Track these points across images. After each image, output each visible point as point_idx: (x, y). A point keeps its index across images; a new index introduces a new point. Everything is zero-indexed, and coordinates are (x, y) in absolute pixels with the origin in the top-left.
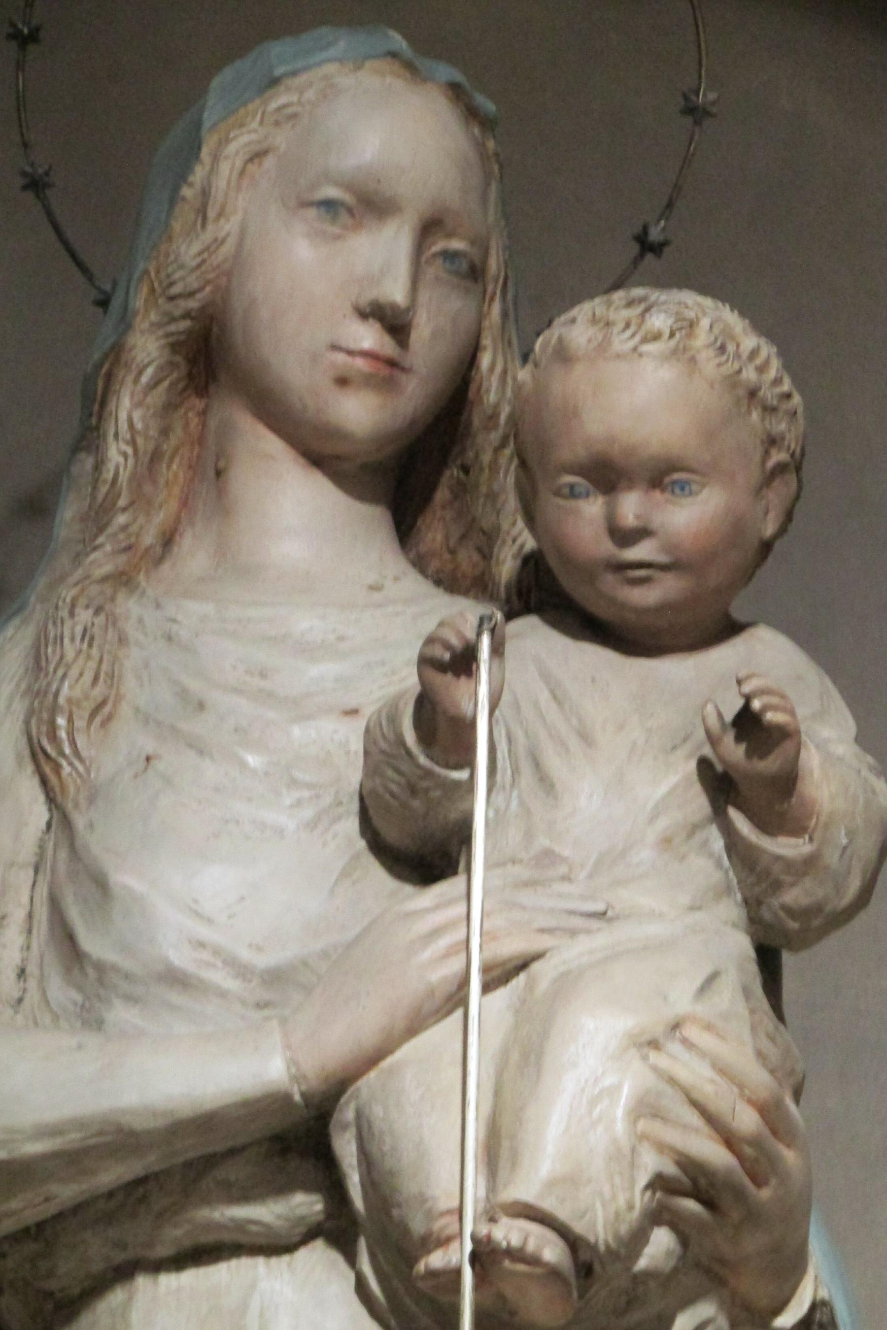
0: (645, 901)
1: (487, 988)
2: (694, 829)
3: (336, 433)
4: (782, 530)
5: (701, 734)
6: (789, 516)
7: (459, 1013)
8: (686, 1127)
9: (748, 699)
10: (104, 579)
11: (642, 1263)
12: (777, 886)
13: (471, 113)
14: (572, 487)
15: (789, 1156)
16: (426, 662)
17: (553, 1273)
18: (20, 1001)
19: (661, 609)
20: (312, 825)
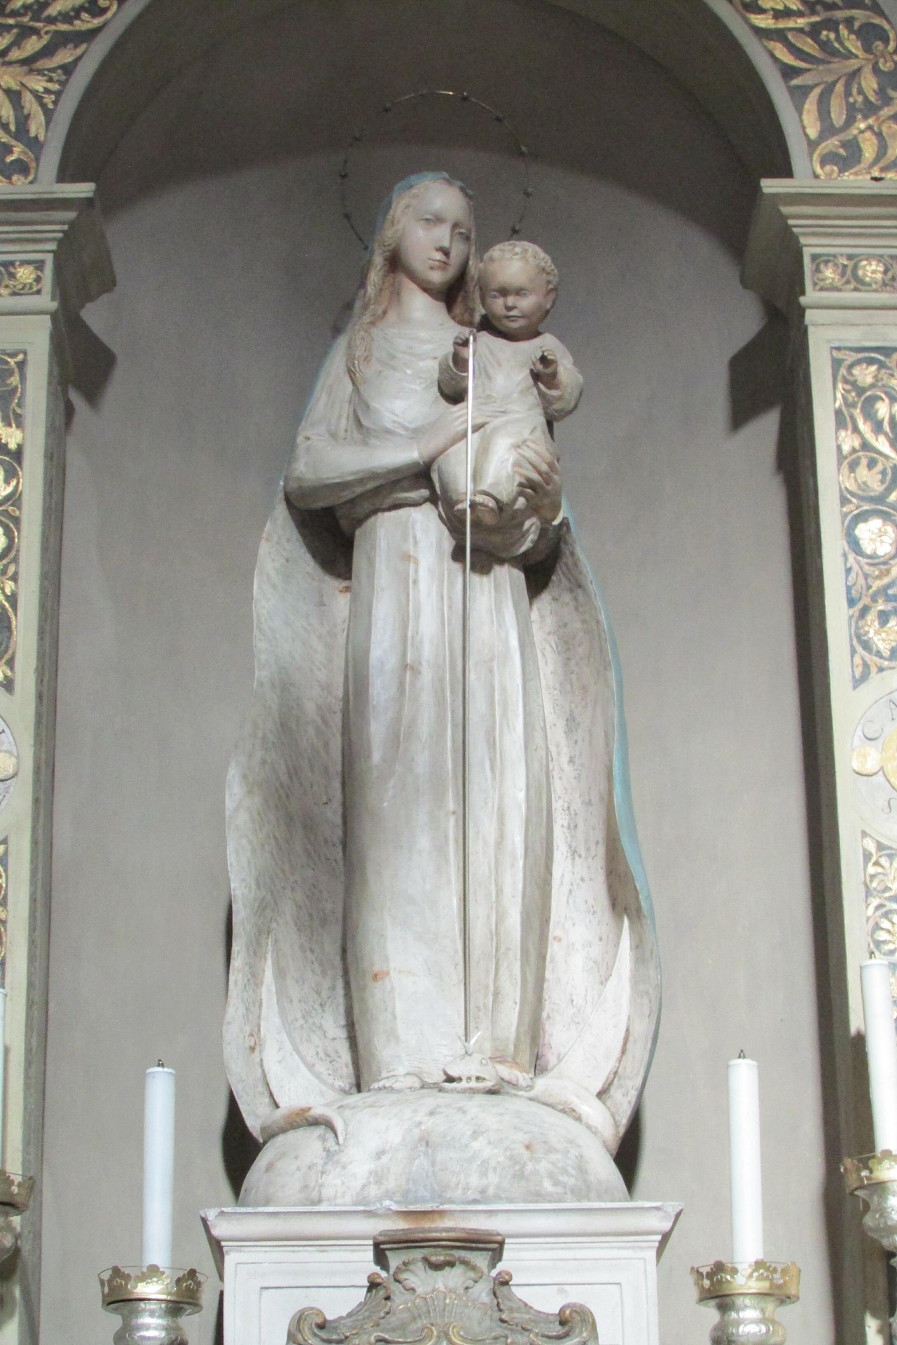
0: (516, 408)
1: (474, 432)
2: (529, 388)
3: (429, 282)
4: (552, 307)
5: (530, 363)
6: (554, 303)
7: (465, 440)
8: (527, 469)
9: (543, 352)
10: (368, 323)
11: (516, 507)
12: (551, 404)
13: (466, 195)
14: (495, 295)
15: (556, 477)
16: (456, 344)
17: (492, 510)
18: (345, 438)
19: (521, 328)
20: (424, 389)
